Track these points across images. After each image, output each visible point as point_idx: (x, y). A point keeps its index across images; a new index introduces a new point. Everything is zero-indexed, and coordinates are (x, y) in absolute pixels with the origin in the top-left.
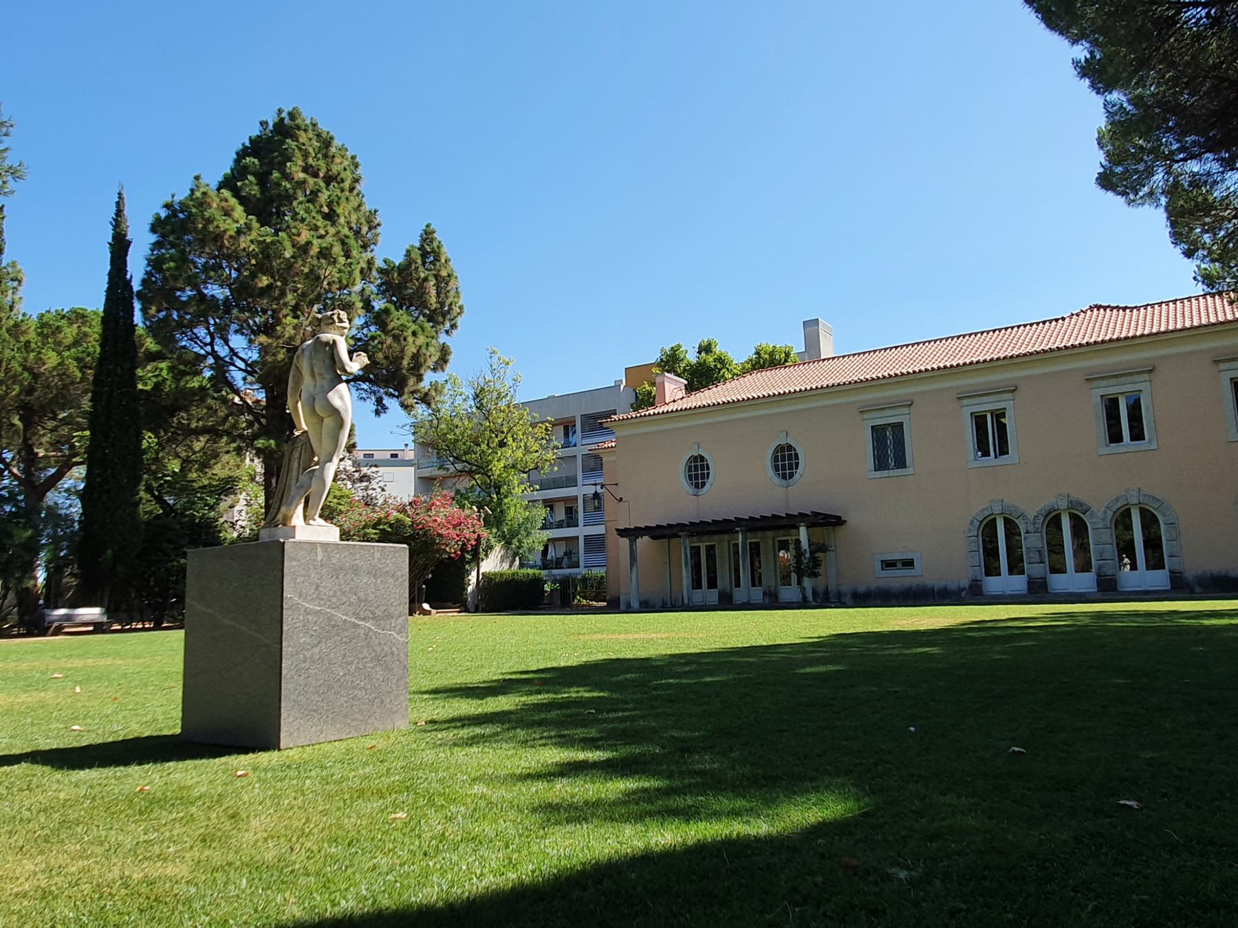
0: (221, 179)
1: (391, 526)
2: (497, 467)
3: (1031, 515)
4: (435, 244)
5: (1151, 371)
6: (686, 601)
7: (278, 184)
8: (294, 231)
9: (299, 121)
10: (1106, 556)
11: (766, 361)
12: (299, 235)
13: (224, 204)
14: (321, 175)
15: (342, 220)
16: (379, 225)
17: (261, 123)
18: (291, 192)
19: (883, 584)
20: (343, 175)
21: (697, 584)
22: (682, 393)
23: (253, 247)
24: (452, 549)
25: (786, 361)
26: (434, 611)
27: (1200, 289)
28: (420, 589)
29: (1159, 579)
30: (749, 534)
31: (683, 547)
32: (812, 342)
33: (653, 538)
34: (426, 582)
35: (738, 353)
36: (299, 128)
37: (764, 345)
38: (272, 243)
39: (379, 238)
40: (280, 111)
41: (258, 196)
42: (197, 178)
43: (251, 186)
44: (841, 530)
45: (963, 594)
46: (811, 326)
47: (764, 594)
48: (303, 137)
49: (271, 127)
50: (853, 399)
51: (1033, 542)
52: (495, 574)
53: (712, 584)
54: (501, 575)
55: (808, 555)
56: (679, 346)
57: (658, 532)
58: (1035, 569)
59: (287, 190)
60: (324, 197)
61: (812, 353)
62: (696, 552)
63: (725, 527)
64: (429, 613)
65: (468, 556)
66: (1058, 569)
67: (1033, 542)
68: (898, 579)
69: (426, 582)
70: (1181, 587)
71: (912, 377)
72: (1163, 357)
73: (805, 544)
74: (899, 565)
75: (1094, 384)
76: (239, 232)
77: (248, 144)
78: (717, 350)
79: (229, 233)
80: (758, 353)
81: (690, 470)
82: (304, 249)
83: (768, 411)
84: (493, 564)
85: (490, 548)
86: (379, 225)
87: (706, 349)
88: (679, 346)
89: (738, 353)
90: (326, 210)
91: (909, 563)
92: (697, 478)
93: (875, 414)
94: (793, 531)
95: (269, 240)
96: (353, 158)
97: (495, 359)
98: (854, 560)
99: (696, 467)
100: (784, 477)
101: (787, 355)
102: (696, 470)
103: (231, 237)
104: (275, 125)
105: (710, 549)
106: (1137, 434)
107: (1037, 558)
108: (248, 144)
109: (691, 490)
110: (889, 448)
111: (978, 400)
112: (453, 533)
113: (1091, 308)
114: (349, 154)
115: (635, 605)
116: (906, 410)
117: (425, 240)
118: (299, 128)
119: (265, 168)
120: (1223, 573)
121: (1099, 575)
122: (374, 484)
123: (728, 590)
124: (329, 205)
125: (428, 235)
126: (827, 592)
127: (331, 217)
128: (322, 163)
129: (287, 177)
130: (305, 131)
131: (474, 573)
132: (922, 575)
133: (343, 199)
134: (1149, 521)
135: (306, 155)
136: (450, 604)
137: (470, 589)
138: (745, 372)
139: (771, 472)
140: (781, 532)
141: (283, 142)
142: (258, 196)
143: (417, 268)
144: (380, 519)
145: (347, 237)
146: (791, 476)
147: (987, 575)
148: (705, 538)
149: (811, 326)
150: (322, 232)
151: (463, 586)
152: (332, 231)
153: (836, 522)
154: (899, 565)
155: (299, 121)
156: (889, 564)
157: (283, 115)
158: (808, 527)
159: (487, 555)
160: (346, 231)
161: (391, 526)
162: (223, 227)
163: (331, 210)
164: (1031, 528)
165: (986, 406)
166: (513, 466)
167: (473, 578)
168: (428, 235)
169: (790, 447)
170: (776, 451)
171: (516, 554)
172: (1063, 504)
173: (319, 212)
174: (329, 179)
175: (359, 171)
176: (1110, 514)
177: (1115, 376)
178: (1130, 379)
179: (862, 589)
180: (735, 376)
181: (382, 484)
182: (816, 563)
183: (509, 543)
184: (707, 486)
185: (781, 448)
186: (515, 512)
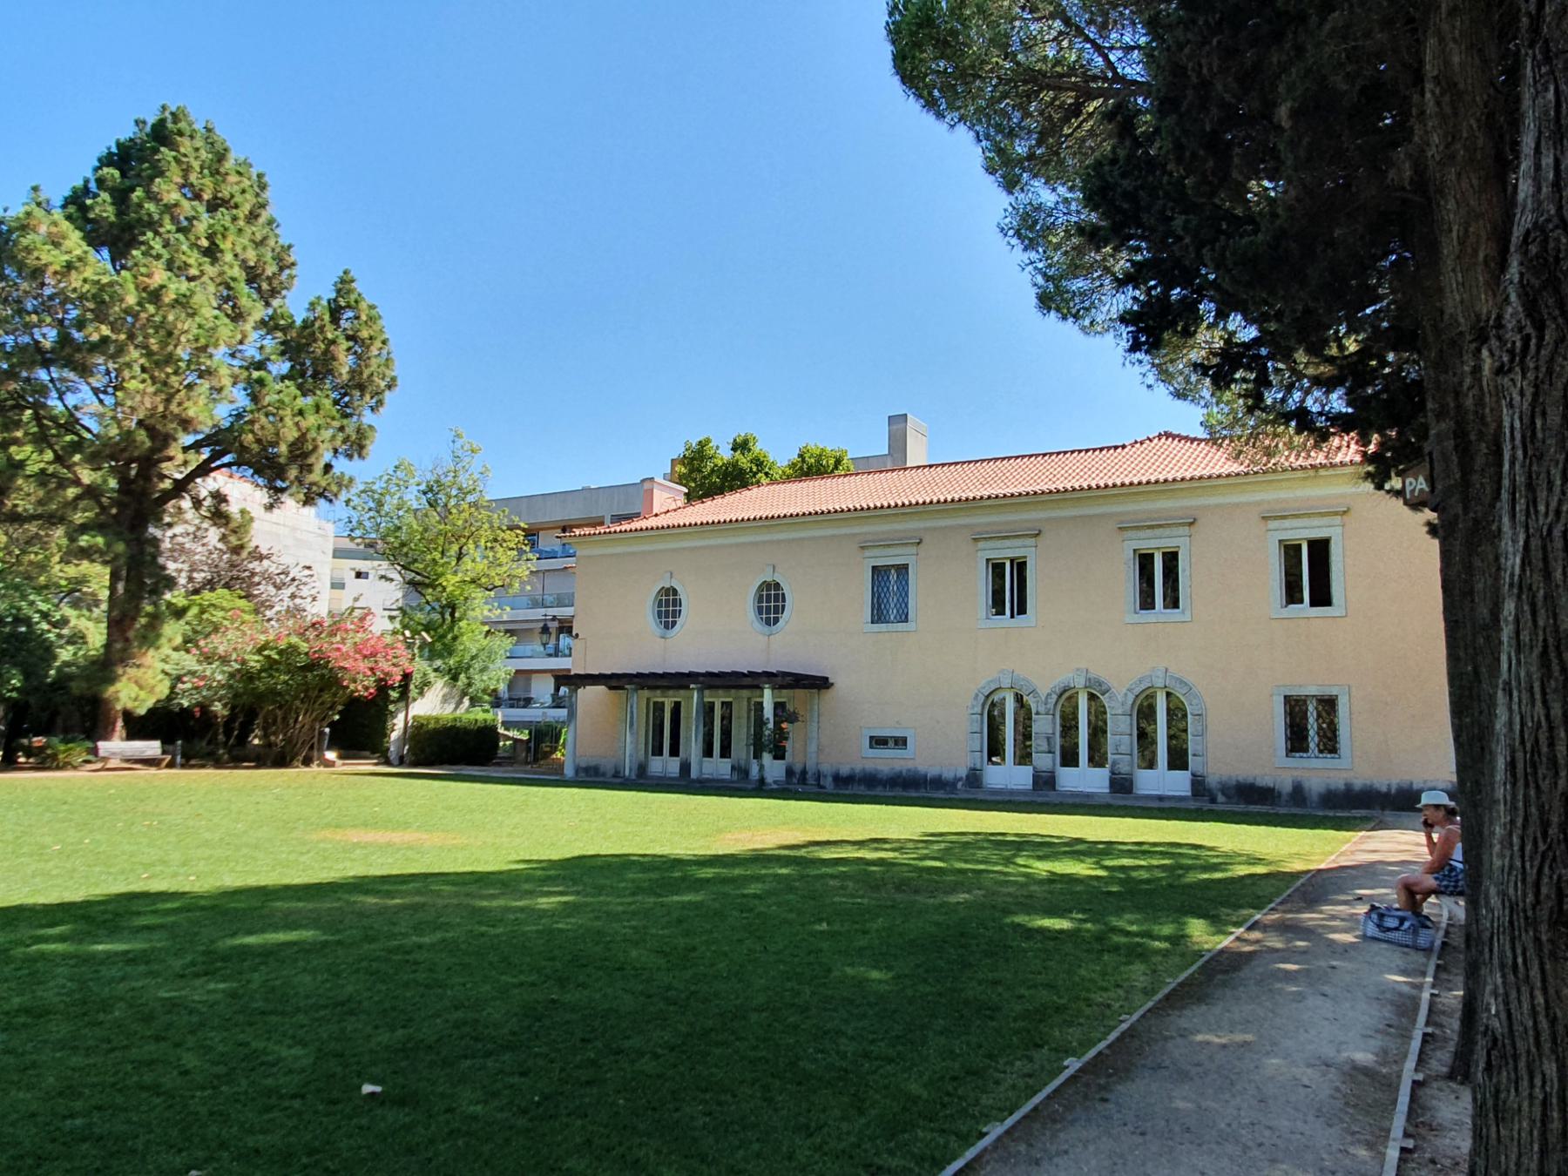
0: (67, 193)
1: (281, 652)
2: (450, 581)
3: (1043, 691)
4: (353, 297)
5: (1191, 524)
6: (694, 774)
7: (140, 206)
8: (143, 270)
9: (182, 125)
10: (1123, 749)
11: (810, 468)
12: (149, 276)
13: (54, 229)
14: (206, 197)
15: (229, 257)
16: (293, 264)
17: (137, 122)
18: (156, 217)
19: (870, 766)
20: (238, 199)
21: (708, 752)
22: (681, 501)
23: (87, 287)
24: (363, 686)
25: (836, 467)
26: (340, 762)
27: (1201, 433)
28: (322, 733)
29: (1177, 783)
30: (707, 692)
31: (640, 700)
32: (898, 443)
33: (611, 688)
34: (332, 725)
35: (781, 456)
36: (180, 133)
37: (811, 446)
38: (111, 284)
39: (296, 281)
40: (164, 108)
41: (113, 218)
42: (35, 189)
43: (103, 206)
44: (828, 695)
45: (959, 785)
46: (898, 423)
47: (733, 768)
48: (186, 146)
49: (148, 129)
50: (857, 530)
51: (1045, 726)
52: (428, 719)
53: (726, 752)
54: (437, 719)
55: (771, 726)
56: (708, 441)
57: (613, 681)
58: (1043, 761)
59: (150, 215)
60: (201, 227)
61: (895, 458)
62: (708, 710)
63: (679, 681)
64: (330, 764)
65: (394, 695)
66: (1070, 759)
67: (1045, 726)
68: (887, 761)
69: (332, 725)
70: (1208, 801)
71: (921, 509)
72: (1048, 520)
73: (768, 712)
74: (891, 744)
75: (1129, 534)
76: (69, 266)
77: (114, 150)
78: (757, 449)
79: (51, 269)
80: (801, 456)
81: (760, 600)
82: (155, 296)
83: (830, 532)
84: (431, 704)
85: (425, 685)
86: (293, 264)
87: (741, 446)
88: (708, 441)
89: (781, 456)
90: (205, 243)
91: (901, 742)
92: (768, 612)
93: (876, 552)
94: (758, 692)
95: (105, 280)
96: (260, 176)
97: (458, 445)
98: (835, 737)
99: (768, 596)
100: (768, 622)
101: (838, 462)
102: (768, 601)
103: (56, 273)
104: (154, 126)
105: (727, 706)
106: (1173, 601)
107: (1045, 747)
108: (114, 150)
109: (659, 630)
110: (889, 595)
111: (999, 544)
112: (363, 665)
113: (1160, 437)
114: (254, 172)
115: (569, 772)
116: (913, 550)
117: (338, 291)
118: (180, 133)
119: (127, 183)
120: (1250, 780)
121: (1113, 773)
122: (305, 592)
123: (743, 763)
124: (210, 237)
125: (344, 284)
126: (804, 772)
127: (212, 253)
128: (208, 181)
129: (153, 197)
130: (192, 137)
131: (401, 716)
132: (918, 759)
133: (233, 229)
134: (1177, 713)
135: (186, 172)
136: (367, 753)
137: (394, 736)
138: (788, 479)
139: (751, 613)
140: (659, 692)
141: (157, 151)
142: (113, 218)
143: (322, 328)
144: (267, 643)
145: (234, 279)
146: (776, 620)
147: (1064, 764)
148: (671, 692)
149: (898, 423)
150: (194, 272)
151: (384, 734)
152: (211, 270)
153: (822, 683)
154: (891, 744)
155: (182, 125)
156: (878, 742)
157: (167, 114)
158: (773, 689)
159: (421, 693)
160: (236, 271)
161: (281, 652)
162: (45, 258)
163: (213, 243)
164: (1042, 709)
165: (1006, 552)
166: (473, 581)
167: (399, 722)
168: (344, 284)
169: (675, 592)
170: (760, 588)
171: (464, 694)
172: (1080, 682)
173: (194, 246)
174: (212, 207)
175: (267, 194)
176: (1131, 698)
177: (1150, 527)
178: (1167, 532)
179: (845, 770)
180: (773, 482)
181: (313, 592)
182: (780, 735)
183: (455, 678)
184: (677, 627)
185: (767, 586)
186: (471, 638)
